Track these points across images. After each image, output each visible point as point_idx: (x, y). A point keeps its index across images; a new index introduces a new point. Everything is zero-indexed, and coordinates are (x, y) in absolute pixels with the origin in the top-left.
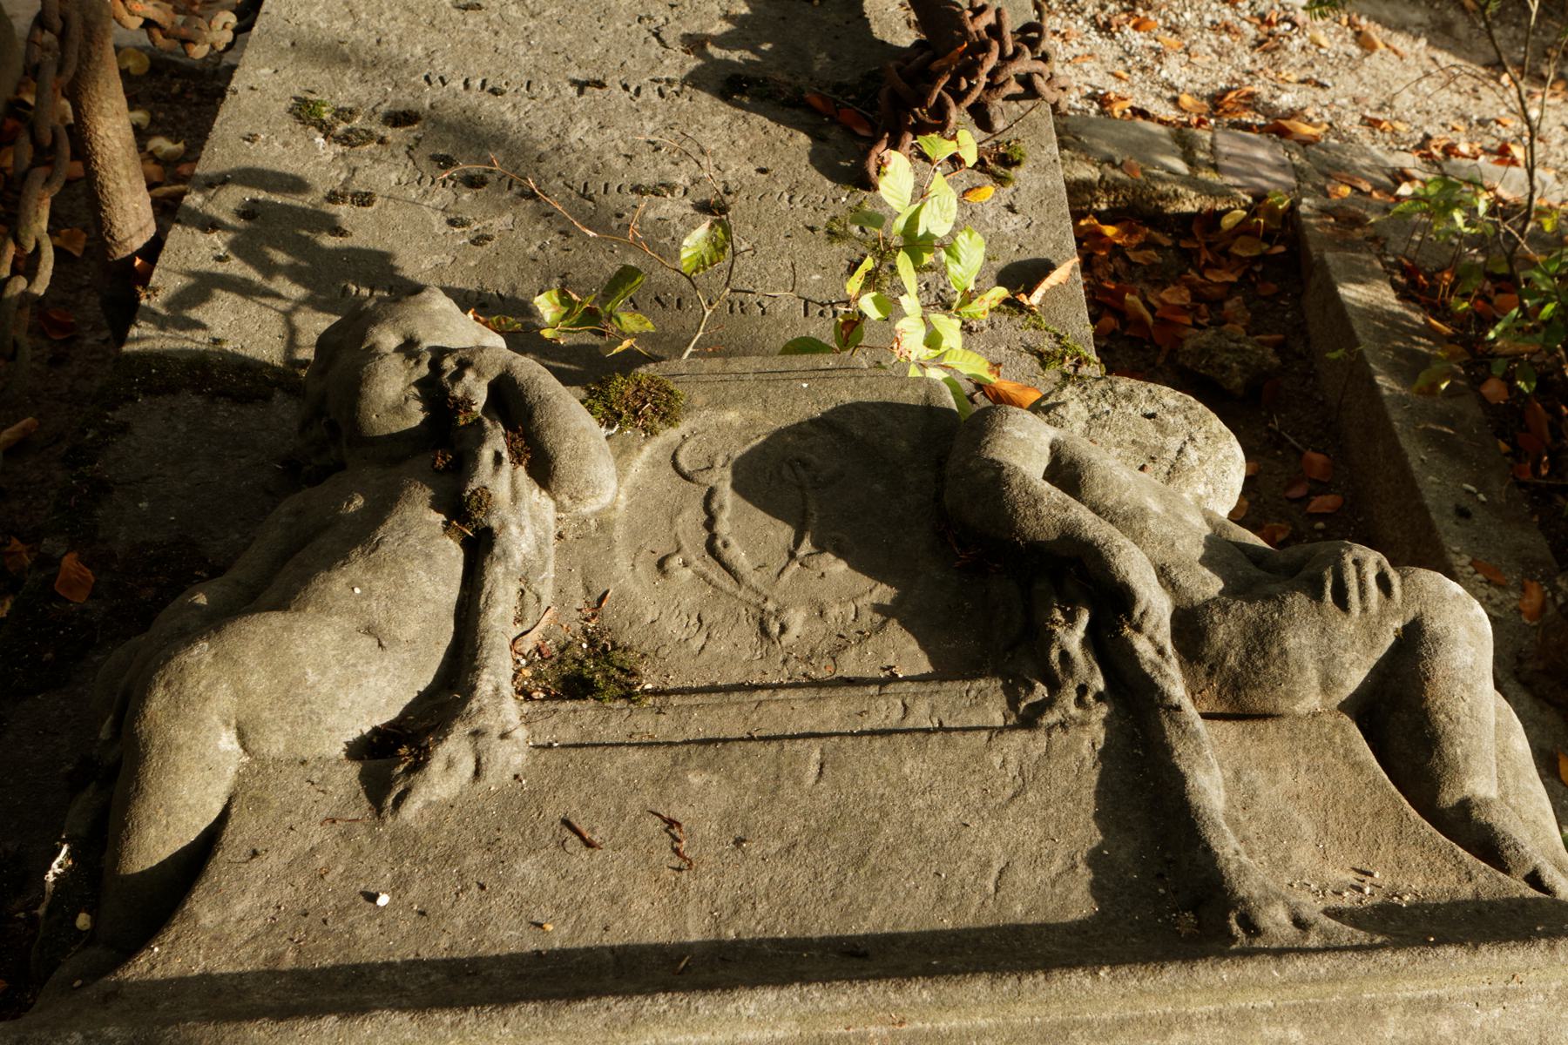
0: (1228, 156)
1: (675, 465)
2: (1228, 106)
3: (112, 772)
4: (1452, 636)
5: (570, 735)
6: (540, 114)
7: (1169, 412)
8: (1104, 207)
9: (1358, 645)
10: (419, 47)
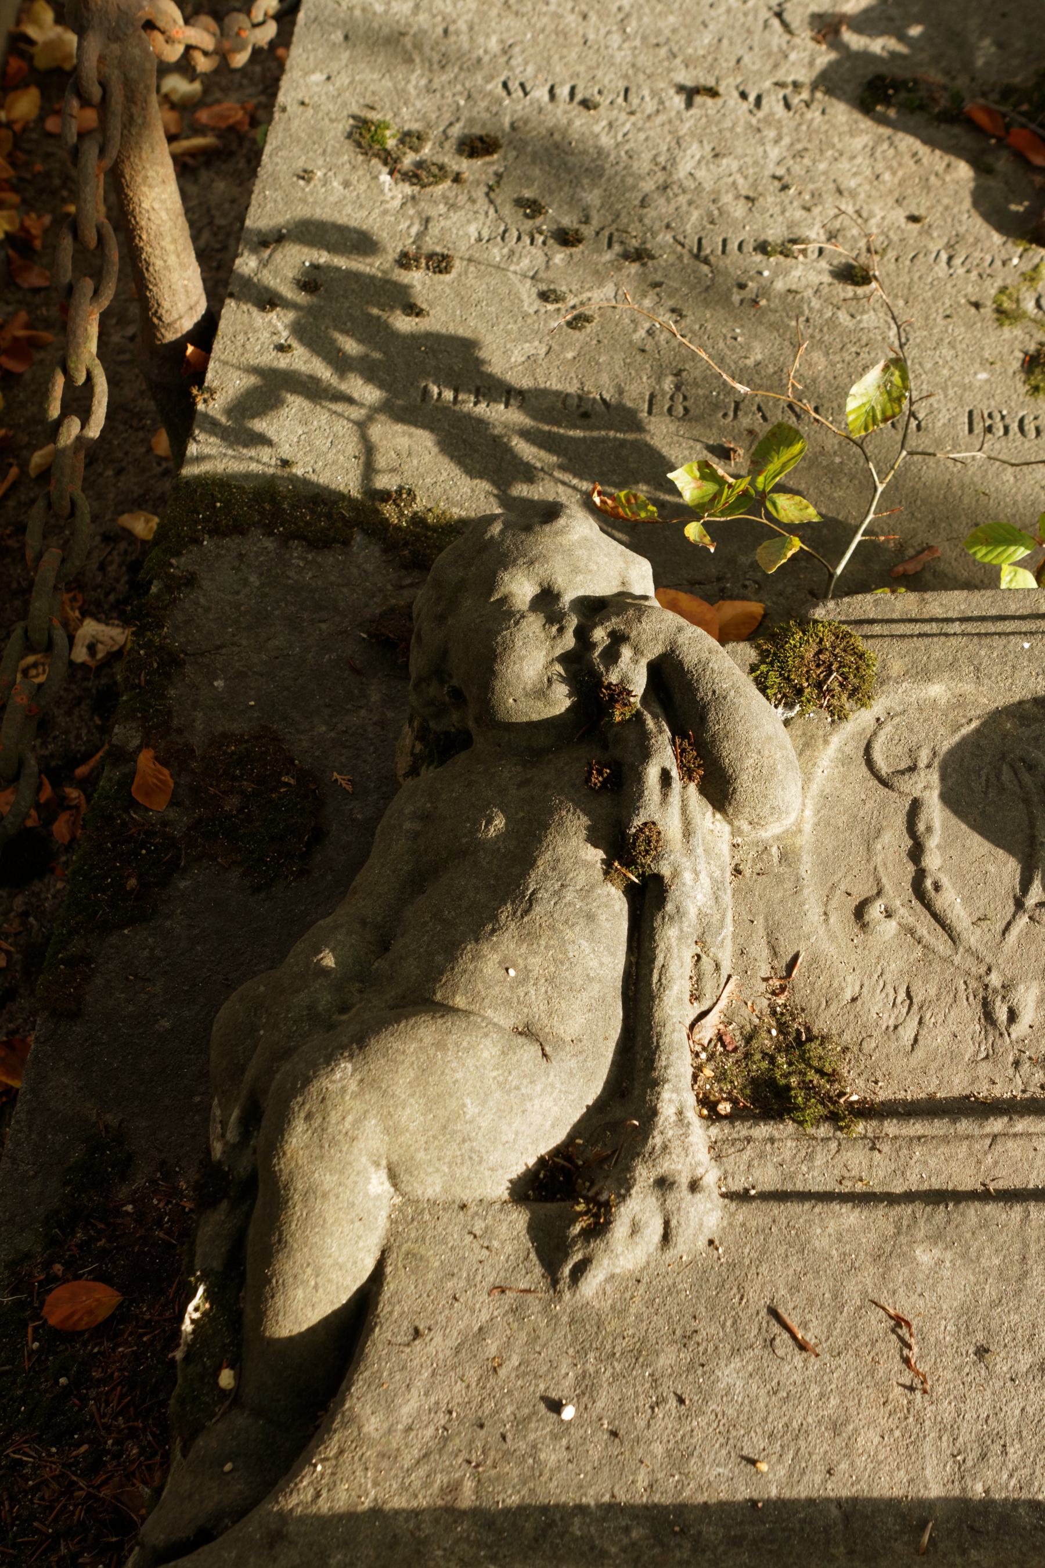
1: (870, 763)
3: (247, 1211)
5: (767, 1178)
6: (642, 136)
10: (494, 39)
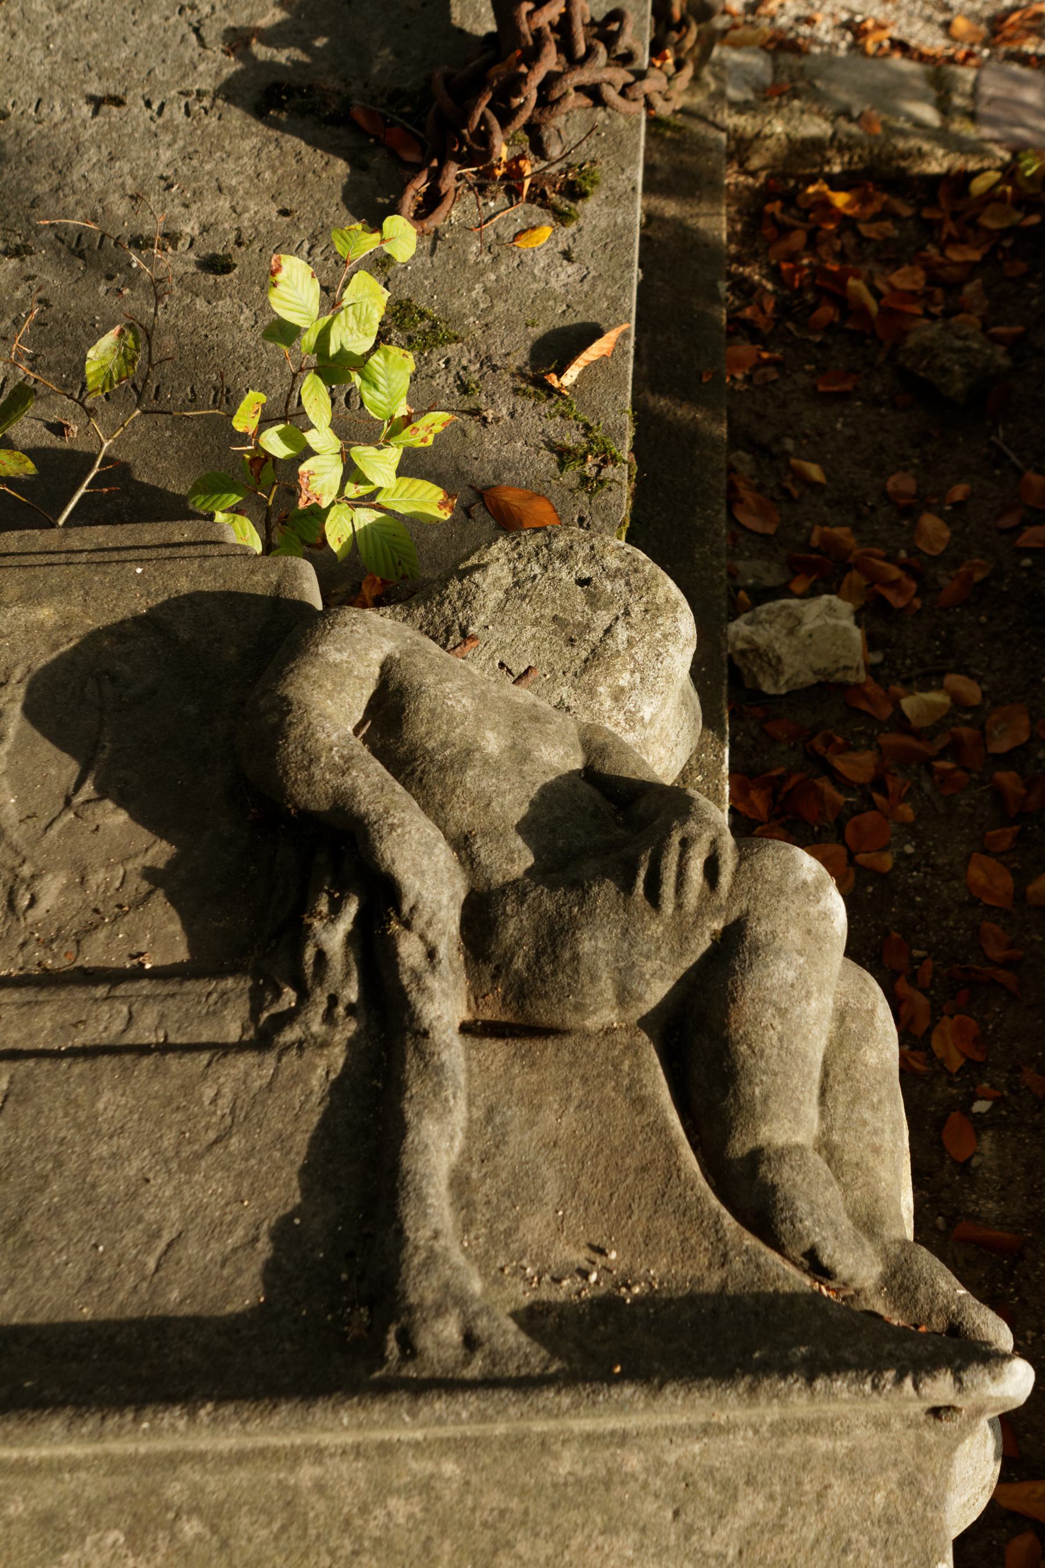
0: (992, 100)
2: (1008, 33)
4: (777, 944)
7: (608, 576)
8: (837, 169)
9: (664, 952)
